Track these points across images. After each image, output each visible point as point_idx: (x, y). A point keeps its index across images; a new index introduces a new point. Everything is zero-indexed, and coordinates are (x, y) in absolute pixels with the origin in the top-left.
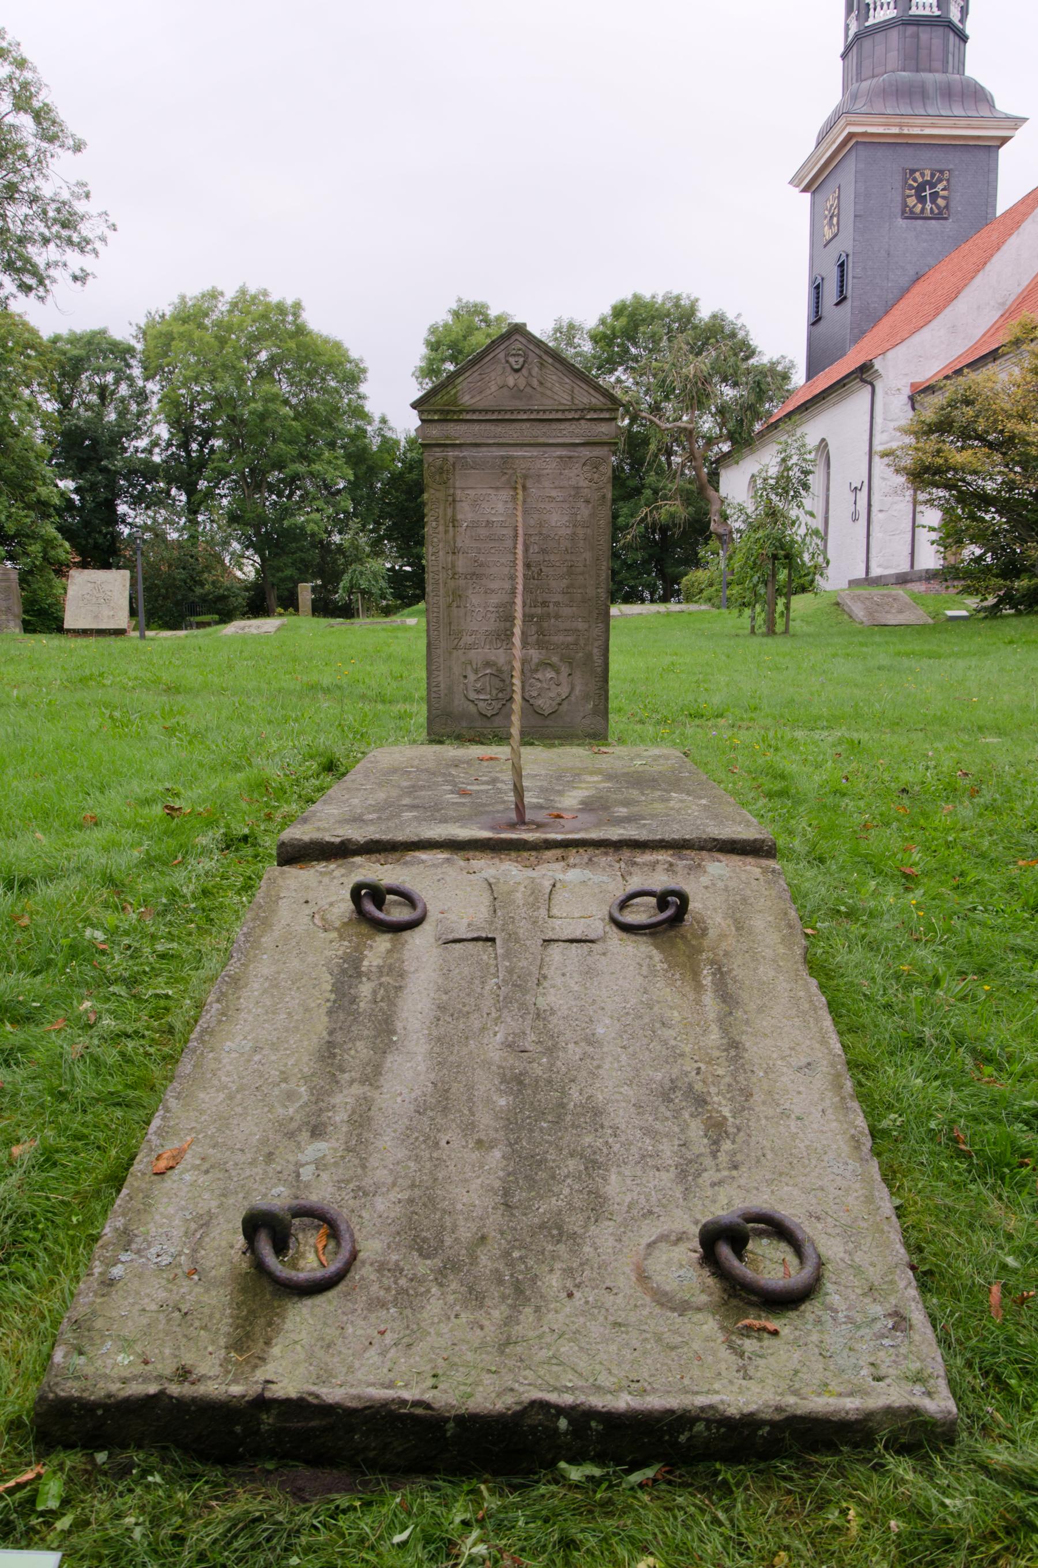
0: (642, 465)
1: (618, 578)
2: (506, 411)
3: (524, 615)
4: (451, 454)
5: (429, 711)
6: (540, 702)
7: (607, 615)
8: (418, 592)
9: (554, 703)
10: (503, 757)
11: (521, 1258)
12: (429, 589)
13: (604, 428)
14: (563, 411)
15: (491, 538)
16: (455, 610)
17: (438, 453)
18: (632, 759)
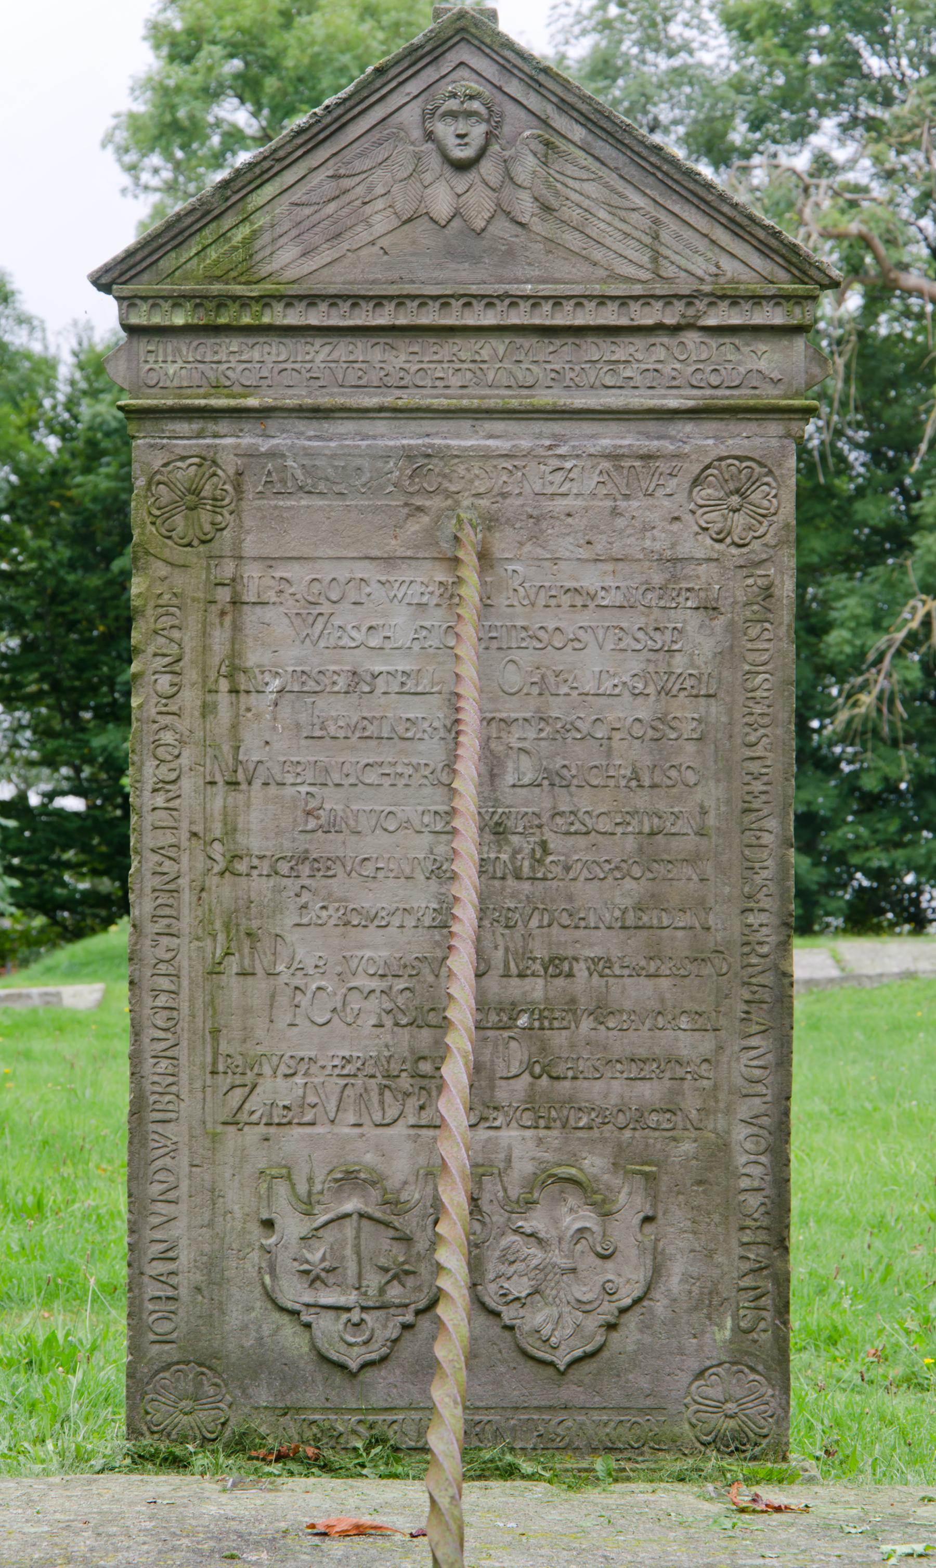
0: (910, 449)
1: (830, 842)
2: (423, 300)
3: (482, 1005)
4: (231, 442)
5: (135, 1348)
6: (538, 1318)
7: (775, 1002)
8: (106, 885)
9: (591, 1323)
10: (404, 1523)
12: (143, 868)
13: (766, 358)
14: (623, 301)
15: (364, 733)
16: (233, 984)
17: (183, 438)
18: (874, 1536)
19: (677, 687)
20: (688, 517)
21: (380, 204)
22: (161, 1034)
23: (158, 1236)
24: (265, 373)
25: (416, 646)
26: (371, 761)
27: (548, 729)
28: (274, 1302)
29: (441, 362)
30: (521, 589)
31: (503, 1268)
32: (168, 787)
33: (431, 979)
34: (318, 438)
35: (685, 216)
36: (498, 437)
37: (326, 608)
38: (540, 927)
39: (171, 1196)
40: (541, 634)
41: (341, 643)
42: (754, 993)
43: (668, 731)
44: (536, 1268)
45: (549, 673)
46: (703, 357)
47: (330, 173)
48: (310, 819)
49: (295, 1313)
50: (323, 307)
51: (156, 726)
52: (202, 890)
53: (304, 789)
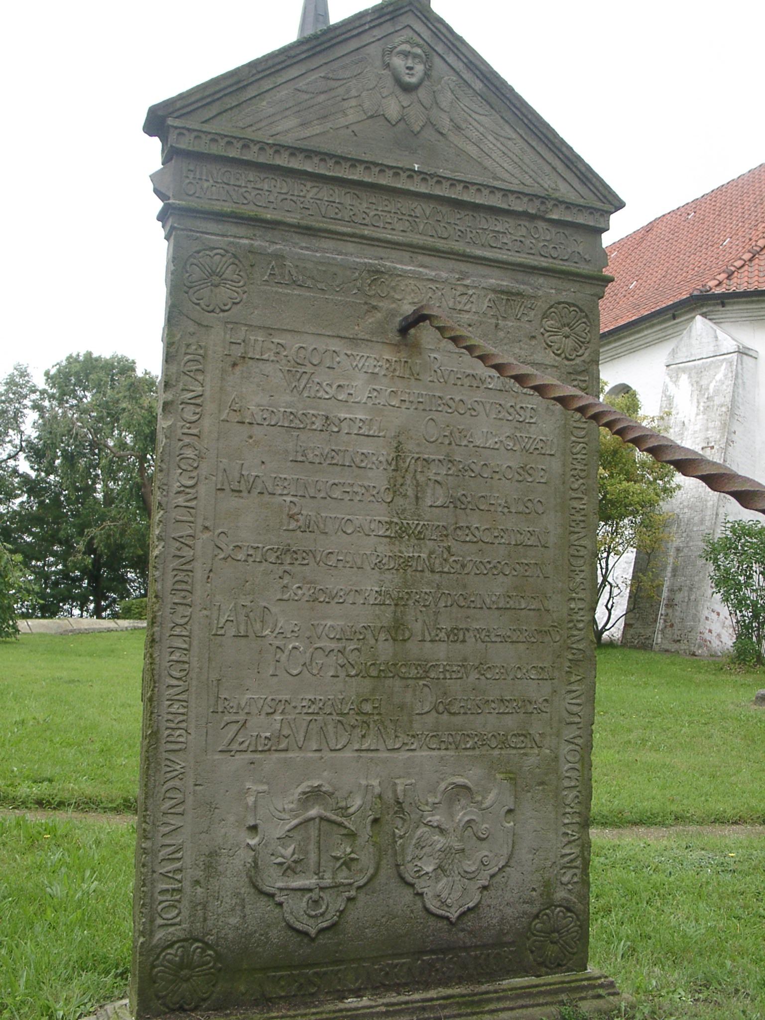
11: (427, 804)
19: (534, 447)
20: (539, 337)
21: (353, 102)
22: (175, 682)
23: (168, 842)
24: (272, 199)
25: (370, 404)
26: (336, 481)
27: (453, 468)
28: (255, 887)
29: (390, 212)
30: (439, 371)
31: (417, 852)
32: (188, 490)
33: (372, 642)
34: (307, 248)
35: (539, 149)
36: (426, 267)
37: (309, 369)
38: (446, 606)
39: (179, 809)
40: (451, 403)
41: (319, 395)
42: (574, 654)
43: (527, 476)
44: (439, 850)
45: (455, 430)
46: (548, 238)
47: (322, 75)
48: (292, 521)
49: (271, 896)
50: (316, 160)
51: (181, 443)
52: (211, 571)
53: (288, 499)
